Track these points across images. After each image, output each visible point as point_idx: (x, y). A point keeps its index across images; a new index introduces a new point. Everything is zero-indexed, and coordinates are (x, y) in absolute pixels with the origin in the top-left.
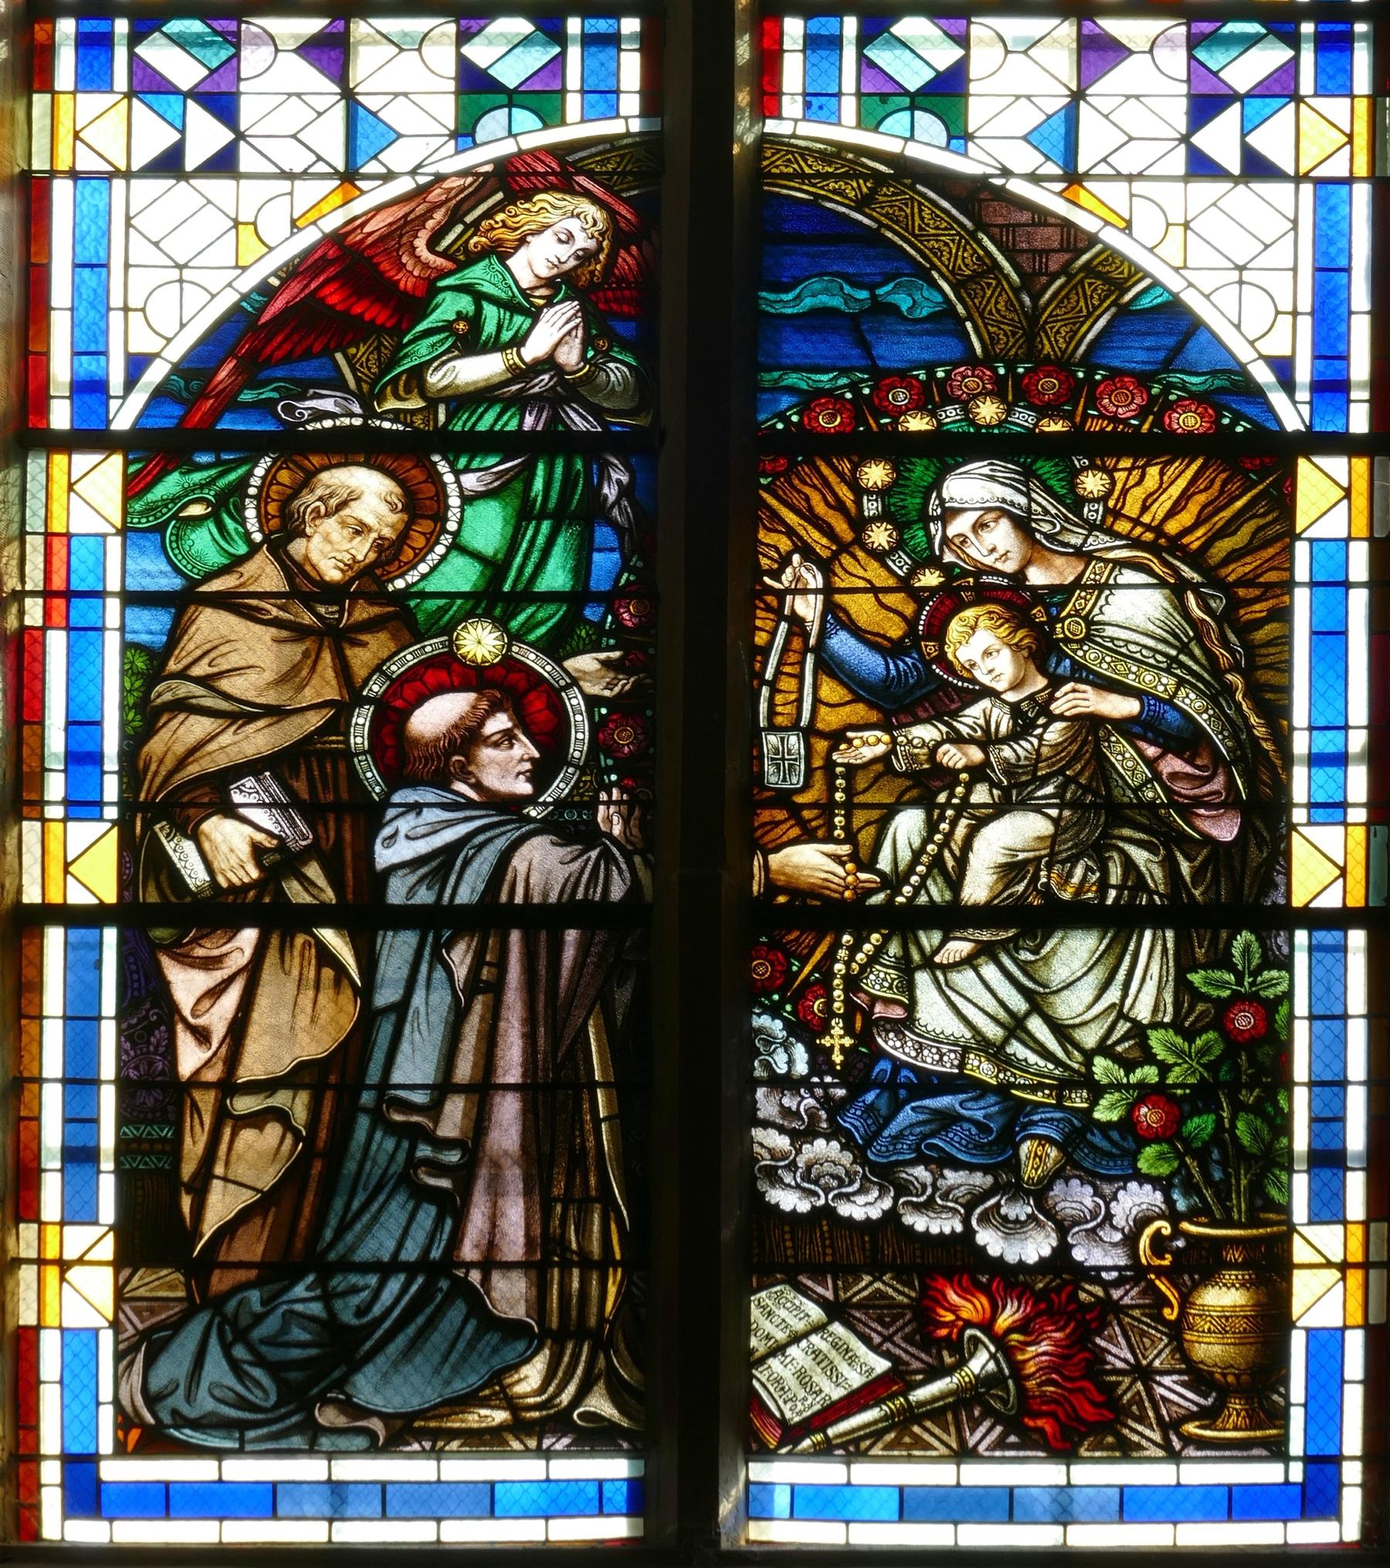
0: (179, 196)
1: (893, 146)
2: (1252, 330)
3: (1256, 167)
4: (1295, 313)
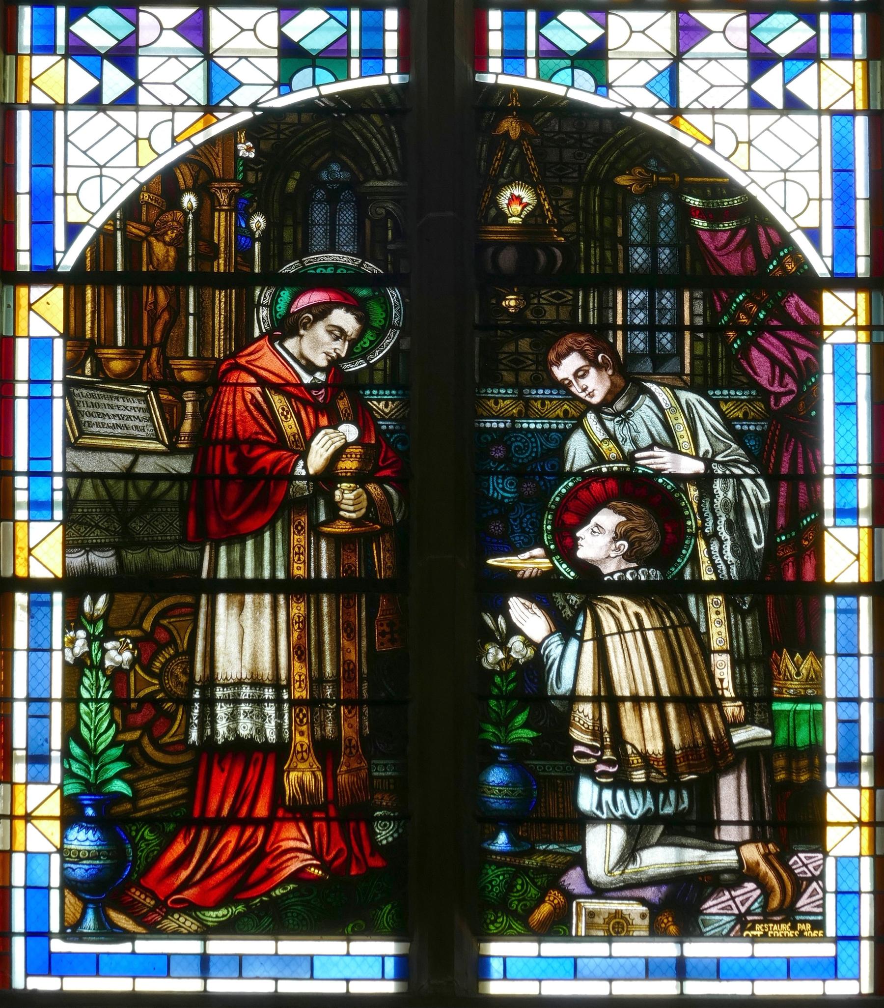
0: (101, 121)
1: (559, 91)
2: (793, 211)
3: (793, 104)
4: (820, 199)
